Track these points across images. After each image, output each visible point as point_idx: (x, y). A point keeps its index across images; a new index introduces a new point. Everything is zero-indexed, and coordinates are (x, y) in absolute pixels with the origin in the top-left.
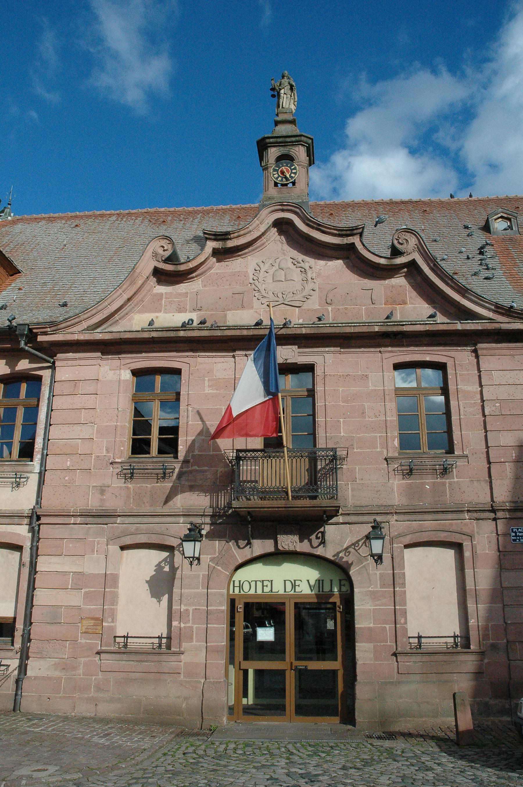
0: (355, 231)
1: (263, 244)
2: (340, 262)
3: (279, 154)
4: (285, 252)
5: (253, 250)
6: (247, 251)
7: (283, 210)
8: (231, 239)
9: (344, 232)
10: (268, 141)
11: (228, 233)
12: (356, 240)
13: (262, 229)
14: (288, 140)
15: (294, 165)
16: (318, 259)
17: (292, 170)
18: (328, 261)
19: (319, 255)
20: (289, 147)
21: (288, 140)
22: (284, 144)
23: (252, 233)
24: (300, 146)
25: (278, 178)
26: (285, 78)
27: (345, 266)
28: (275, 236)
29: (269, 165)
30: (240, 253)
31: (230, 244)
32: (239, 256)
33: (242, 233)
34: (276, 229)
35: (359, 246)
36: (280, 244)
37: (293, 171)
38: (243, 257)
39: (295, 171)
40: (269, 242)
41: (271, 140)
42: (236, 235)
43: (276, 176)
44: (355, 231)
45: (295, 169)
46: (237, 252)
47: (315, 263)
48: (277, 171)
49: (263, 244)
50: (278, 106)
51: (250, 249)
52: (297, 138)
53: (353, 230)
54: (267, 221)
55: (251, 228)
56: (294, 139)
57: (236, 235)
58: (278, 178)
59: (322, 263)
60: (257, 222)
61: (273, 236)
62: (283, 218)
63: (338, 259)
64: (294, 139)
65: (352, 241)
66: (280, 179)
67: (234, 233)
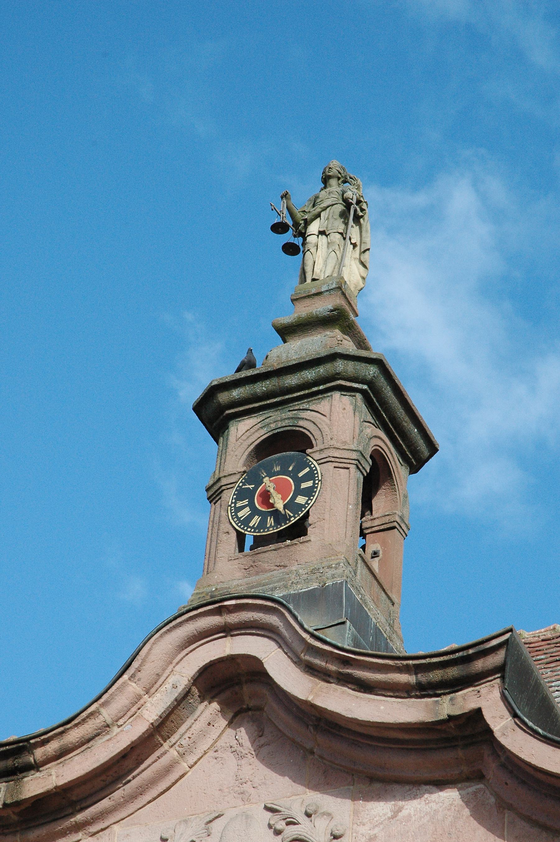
0: (479, 665)
1: (168, 770)
2: (450, 797)
3: (261, 434)
4: (247, 787)
5: (133, 797)
6: (105, 803)
7: (227, 630)
8: (36, 767)
9: (436, 676)
10: (223, 397)
11: (22, 746)
12: (488, 700)
13: (153, 710)
14: (292, 380)
15: (306, 464)
16: (368, 797)
17: (298, 482)
18: (403, 798)
19: (372, 779)
20: (297, 405)
21: (292, 380)
22: (281, 399)
23: (116, 730)
24: (337, 395)
25: (249, 518)
26: (333, 182)
27: (467, 812)
28: (214, 733)
29: (224, 481)
30: (79, 817)
31: (34, 785)
32: (78, 827)
33: (74, 735)
34: (215, 706)
35: (499, 720)
36: (231, 761)
37: (304, 485)
38: (93, 829)
39: (310, 484)
40: (191, 759)
41: (236, 393)
42: (52, 747)
43: (244, 513)
44: (479, 665)
45: (311, 476)
46: (72, 814)
47: (356, 813)
48: (249, 495)
49: (168, 770)
50: (303, 279)
51: (118, 795)
52: (321, 370)
53: (468, 659)
54: (171, 680)
55: (107, 715)
56: (309, 375)
57: (52, 747)
58: (249, 518)
59: (380, 809)
60: (134, 688)
61: (203, 734)
62: (232, 659)
63: (440, 784)
64: (309, 375)
65: (472, 705)
66: (256, 520)
67: (44, 743)
